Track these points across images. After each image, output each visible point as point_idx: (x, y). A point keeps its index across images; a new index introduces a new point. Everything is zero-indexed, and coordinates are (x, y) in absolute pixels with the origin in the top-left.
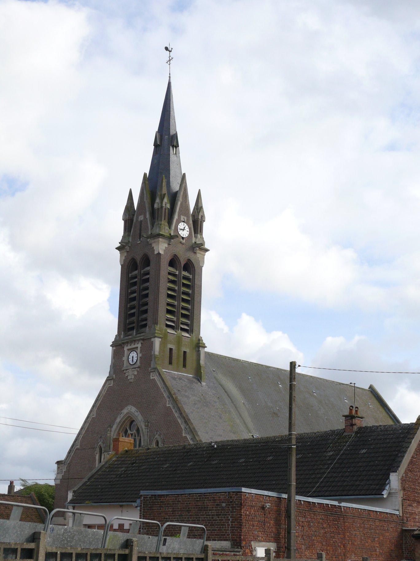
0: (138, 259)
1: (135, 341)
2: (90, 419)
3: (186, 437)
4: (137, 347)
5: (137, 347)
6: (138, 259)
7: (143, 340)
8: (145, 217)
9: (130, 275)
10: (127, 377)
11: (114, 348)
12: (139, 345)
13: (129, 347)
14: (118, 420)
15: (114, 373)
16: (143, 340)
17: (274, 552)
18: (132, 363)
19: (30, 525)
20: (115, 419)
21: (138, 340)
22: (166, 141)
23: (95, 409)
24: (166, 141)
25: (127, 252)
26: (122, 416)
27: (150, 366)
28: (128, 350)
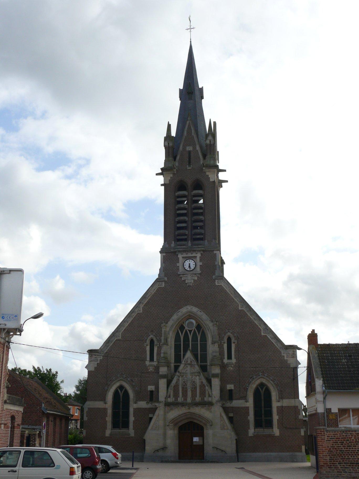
0: (189, 182)
1: (195, 251)
2: (134, 315)
3: (266, 336)
4: (196, 257)
5: (196, 257)
6: (189, 182)
7: (203, 251)
8: (195, 148)
9: (176, 194)
10: (185, 280)
11: (164, 254)
12: (199, 255)
13: (185, 255)
14: (175, 317)
15: (165, 276)
16: (203, 251)
17: (189, 409)
18: (188, 269)
19: (21, 411)
20: (171, 316)
21: (200, 251)
22: (191, 94)
23: (142, 306)
24: (191, 94)
25: (174, 174)
26: (180, 314)
27: (214, 274)
28: (183, 257)
